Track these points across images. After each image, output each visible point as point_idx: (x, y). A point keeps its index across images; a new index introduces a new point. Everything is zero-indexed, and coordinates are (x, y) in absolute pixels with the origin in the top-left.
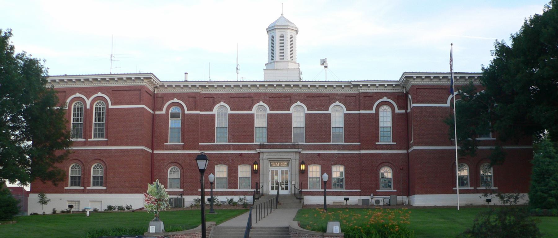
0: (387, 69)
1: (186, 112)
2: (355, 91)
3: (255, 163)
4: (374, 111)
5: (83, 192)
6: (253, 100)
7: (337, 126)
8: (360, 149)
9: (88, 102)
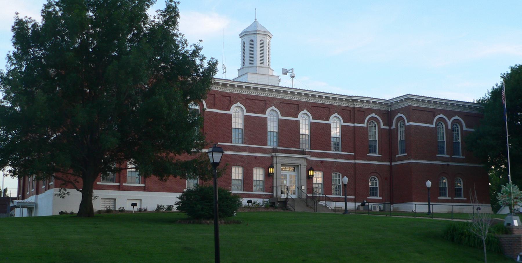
0: (385, 88)
2: (350, 105)
4: (365, 125)
5: (119, 188)
6: (266, 104)
7: (237, 127)
8: (355, 159)
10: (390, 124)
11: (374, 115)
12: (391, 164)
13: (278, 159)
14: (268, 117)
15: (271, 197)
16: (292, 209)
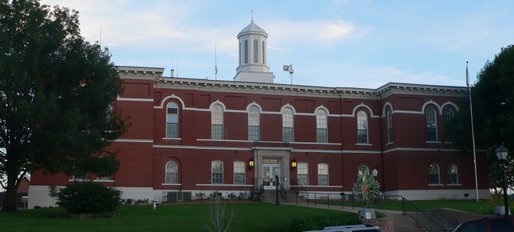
0: (370, 78)
1: (184, 108)
2: (336, 96)
3: (252, 160)
4: (353, 115)
7: (288, 126)
8: (342, 149)
9: (441, 109)
10: (380, 114)
11: (362, 105)
12: (382, 152)
13: (259, 152)
14: (249, 113)
15: (252, 189)
16: (262, 200)
